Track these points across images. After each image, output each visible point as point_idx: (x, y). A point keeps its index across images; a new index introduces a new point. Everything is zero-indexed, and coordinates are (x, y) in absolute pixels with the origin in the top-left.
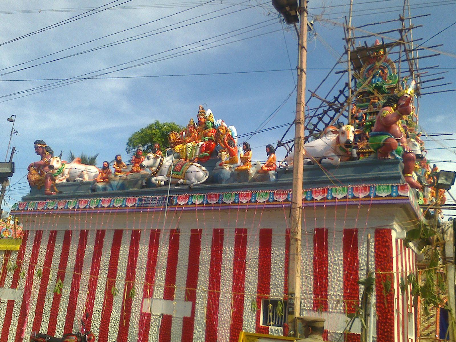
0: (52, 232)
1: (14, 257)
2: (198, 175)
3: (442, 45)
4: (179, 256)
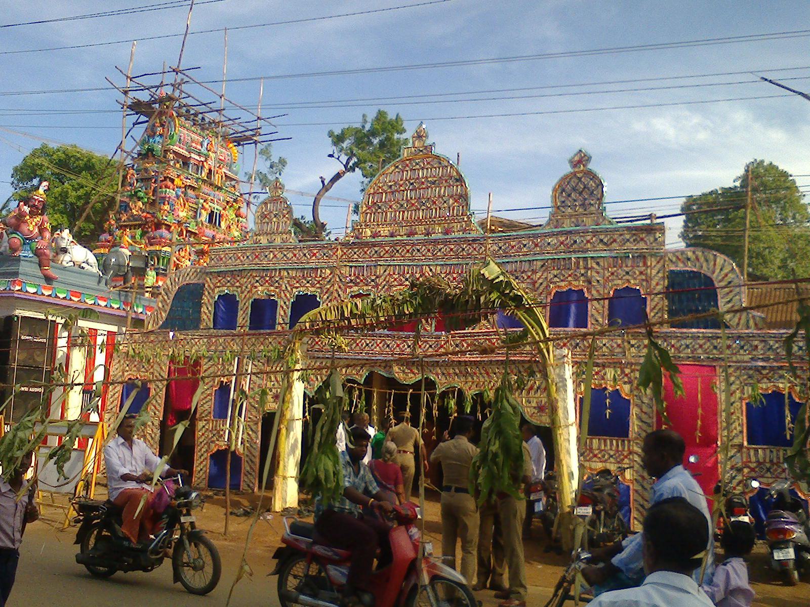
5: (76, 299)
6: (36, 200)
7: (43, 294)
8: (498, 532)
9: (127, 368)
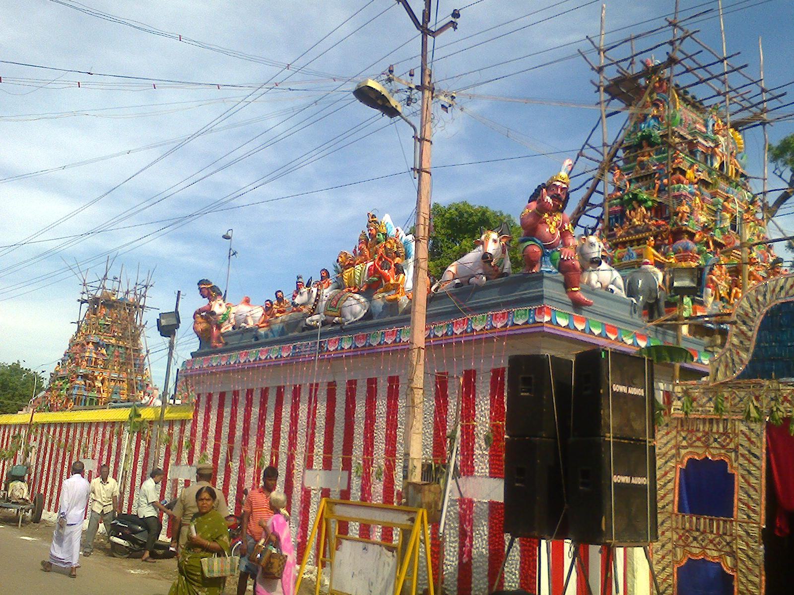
0: (330, 384)
1: (188, 427)
2: (354, 311)
3: (739, 53)
4: (336, 415)
5: (613, 337)
6: (557, 187)
7: (576, 329)
8: (606, 574)
9: (684, 443)
